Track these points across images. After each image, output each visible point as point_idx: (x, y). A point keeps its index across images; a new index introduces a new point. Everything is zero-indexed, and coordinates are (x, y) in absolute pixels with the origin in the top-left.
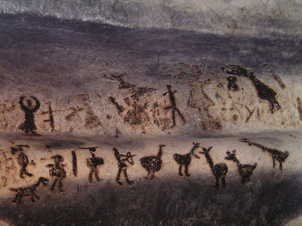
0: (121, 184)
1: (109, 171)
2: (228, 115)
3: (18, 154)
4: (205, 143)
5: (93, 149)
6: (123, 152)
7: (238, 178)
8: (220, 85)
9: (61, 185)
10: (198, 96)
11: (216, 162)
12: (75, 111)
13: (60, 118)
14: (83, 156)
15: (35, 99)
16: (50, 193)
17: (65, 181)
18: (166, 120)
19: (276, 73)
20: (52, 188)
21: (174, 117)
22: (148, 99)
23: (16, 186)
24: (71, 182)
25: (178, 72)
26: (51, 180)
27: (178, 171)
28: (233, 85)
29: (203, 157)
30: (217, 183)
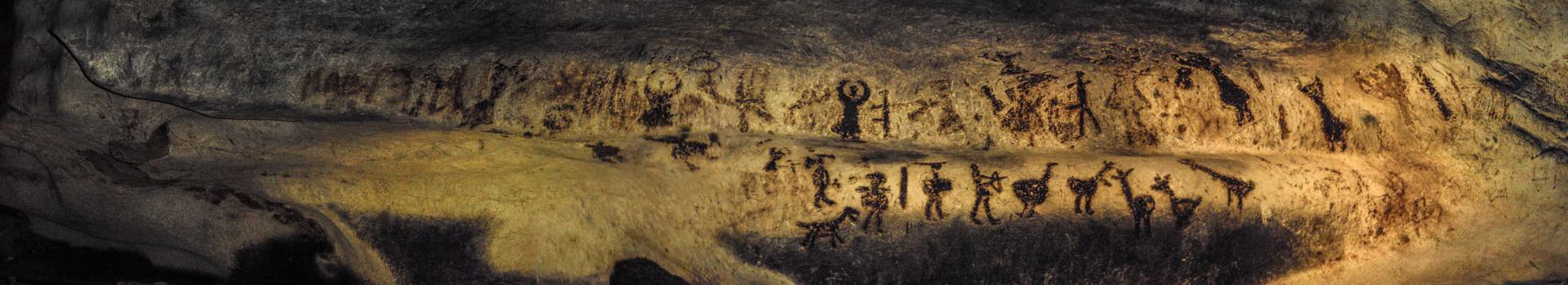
0: (978, 222)
1: (960, 200)
2: (1170, 123)
3: (815, 167)
4: (1123, 163)
5: (937, 166)
6: (986, 171)
7: (1171, 219)
8: (1164, 79)
9: (879, 221)
10: (1126, 92)
11: (1137, 192)
12: (925, 105)
14: (918, 176)
15: (864, 84)
16: (861, 234)
17: (888, 214)
18: (1069, 126)
19: (1254, 68)
20: (865, 227)
21: (1081, 122)
22: (1043, 92)
23: (807, 220)
24: (895, 217)
25: (1104, 56)
26: (864, 211)
27: (1073, 206)
28: (1184, 81)
29: (1116, 185)
30: (1137, 226)
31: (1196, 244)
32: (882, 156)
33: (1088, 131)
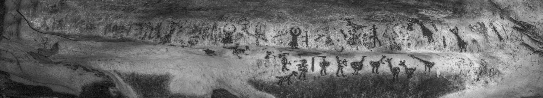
0: (339, 76)
1: (332, 69)
2: (405, 42)
3: (282, 57)
4: (389, 56)
5: (324, 57)
7: (406, 75)
8: (403, 27)
9: (305, 76)
10: (390, 32)
11: (394, 66)
12: (320, 36)
13: (312, 40)
14: (318, 60)
15: (299, 29)
16: (298, 80)
17: (307, 74)
18: (370, 43)
20: (300, 78)
21: (374, 42)
22: (361, 31)
23: (279, 76)
24: (310, 75)
25: (382, 19)
26: (299, 73)
27: (372, 71)
28: (410, 28)
29: (387, 63)
30: (394, 78)
31: (414, 84)
32: (306, 54)
33: (377, 45)
